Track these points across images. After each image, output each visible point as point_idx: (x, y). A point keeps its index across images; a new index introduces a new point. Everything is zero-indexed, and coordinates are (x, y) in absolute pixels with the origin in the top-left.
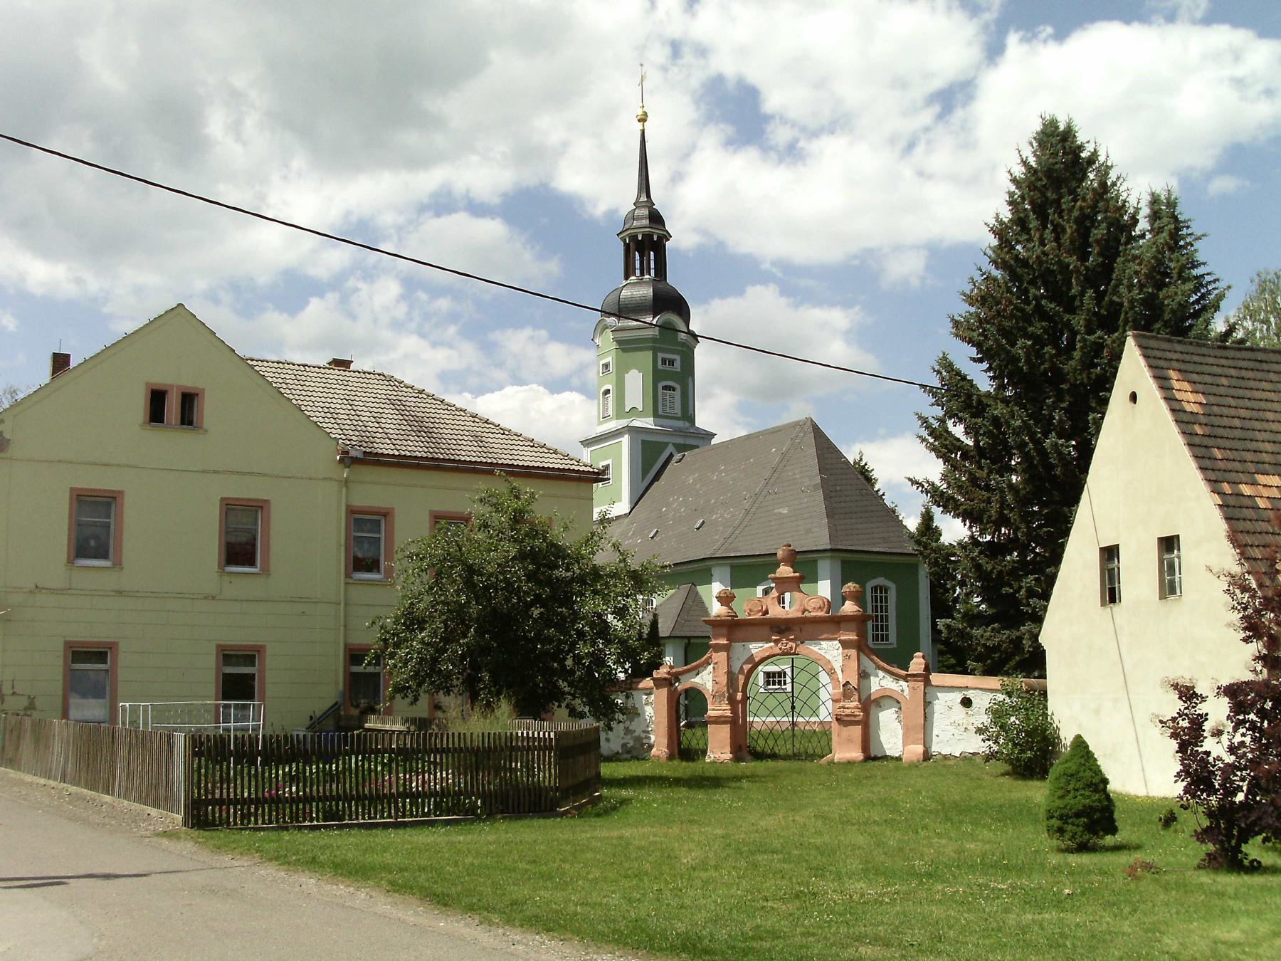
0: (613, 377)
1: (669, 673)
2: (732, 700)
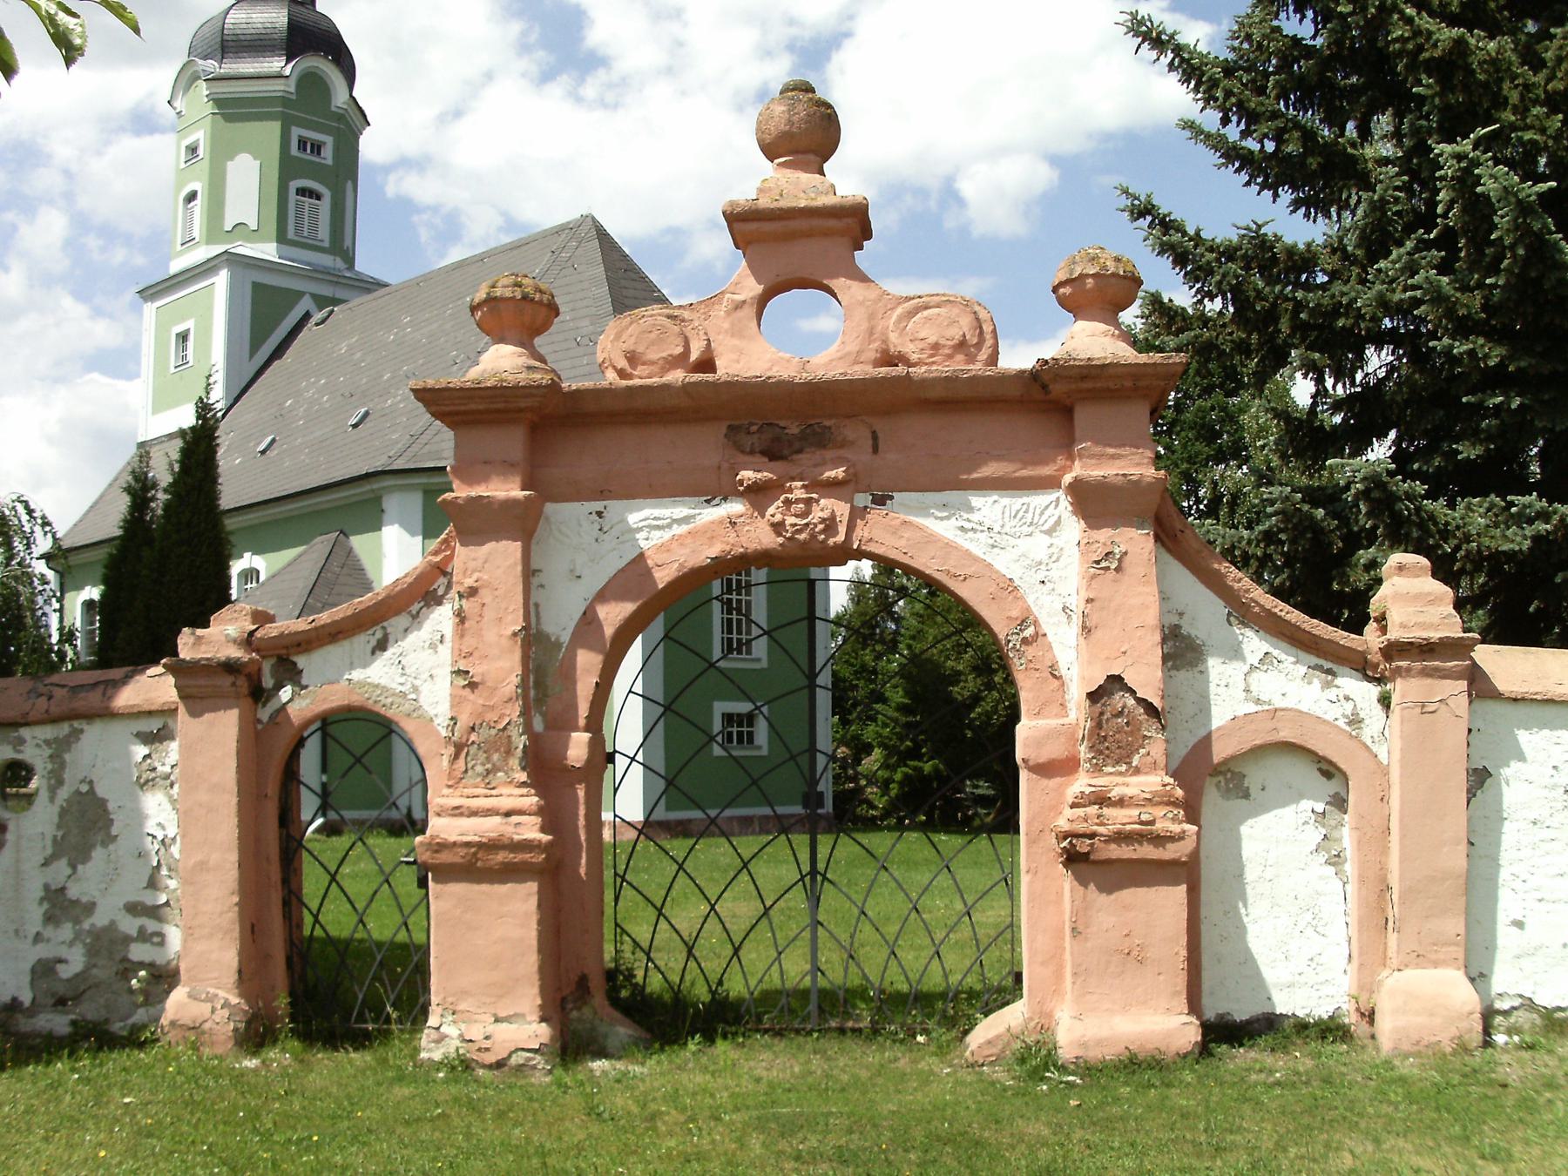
0: (203, 166)
1: (248, 641)
2: (544, 769)
